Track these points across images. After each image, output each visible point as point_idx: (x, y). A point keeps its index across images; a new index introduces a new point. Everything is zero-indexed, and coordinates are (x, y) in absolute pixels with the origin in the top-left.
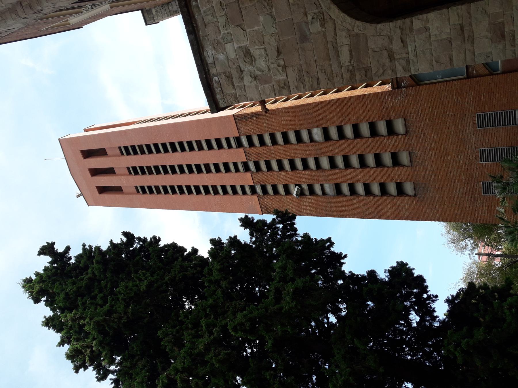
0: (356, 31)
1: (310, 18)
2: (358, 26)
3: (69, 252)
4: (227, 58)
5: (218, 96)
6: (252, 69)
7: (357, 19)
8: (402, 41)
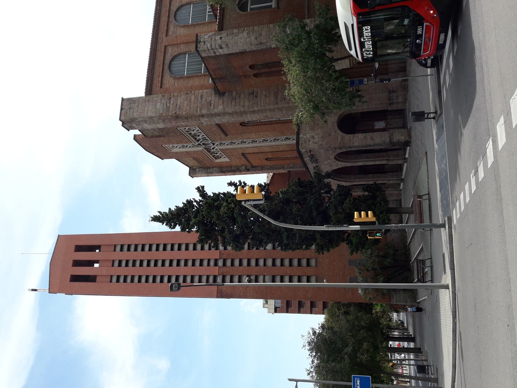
0: (343, 135)
1: (332, 131)
3: (175, 209)
5: (300, 146)
6: (313, 140)
7: (343, 133)
8: (353, 138)
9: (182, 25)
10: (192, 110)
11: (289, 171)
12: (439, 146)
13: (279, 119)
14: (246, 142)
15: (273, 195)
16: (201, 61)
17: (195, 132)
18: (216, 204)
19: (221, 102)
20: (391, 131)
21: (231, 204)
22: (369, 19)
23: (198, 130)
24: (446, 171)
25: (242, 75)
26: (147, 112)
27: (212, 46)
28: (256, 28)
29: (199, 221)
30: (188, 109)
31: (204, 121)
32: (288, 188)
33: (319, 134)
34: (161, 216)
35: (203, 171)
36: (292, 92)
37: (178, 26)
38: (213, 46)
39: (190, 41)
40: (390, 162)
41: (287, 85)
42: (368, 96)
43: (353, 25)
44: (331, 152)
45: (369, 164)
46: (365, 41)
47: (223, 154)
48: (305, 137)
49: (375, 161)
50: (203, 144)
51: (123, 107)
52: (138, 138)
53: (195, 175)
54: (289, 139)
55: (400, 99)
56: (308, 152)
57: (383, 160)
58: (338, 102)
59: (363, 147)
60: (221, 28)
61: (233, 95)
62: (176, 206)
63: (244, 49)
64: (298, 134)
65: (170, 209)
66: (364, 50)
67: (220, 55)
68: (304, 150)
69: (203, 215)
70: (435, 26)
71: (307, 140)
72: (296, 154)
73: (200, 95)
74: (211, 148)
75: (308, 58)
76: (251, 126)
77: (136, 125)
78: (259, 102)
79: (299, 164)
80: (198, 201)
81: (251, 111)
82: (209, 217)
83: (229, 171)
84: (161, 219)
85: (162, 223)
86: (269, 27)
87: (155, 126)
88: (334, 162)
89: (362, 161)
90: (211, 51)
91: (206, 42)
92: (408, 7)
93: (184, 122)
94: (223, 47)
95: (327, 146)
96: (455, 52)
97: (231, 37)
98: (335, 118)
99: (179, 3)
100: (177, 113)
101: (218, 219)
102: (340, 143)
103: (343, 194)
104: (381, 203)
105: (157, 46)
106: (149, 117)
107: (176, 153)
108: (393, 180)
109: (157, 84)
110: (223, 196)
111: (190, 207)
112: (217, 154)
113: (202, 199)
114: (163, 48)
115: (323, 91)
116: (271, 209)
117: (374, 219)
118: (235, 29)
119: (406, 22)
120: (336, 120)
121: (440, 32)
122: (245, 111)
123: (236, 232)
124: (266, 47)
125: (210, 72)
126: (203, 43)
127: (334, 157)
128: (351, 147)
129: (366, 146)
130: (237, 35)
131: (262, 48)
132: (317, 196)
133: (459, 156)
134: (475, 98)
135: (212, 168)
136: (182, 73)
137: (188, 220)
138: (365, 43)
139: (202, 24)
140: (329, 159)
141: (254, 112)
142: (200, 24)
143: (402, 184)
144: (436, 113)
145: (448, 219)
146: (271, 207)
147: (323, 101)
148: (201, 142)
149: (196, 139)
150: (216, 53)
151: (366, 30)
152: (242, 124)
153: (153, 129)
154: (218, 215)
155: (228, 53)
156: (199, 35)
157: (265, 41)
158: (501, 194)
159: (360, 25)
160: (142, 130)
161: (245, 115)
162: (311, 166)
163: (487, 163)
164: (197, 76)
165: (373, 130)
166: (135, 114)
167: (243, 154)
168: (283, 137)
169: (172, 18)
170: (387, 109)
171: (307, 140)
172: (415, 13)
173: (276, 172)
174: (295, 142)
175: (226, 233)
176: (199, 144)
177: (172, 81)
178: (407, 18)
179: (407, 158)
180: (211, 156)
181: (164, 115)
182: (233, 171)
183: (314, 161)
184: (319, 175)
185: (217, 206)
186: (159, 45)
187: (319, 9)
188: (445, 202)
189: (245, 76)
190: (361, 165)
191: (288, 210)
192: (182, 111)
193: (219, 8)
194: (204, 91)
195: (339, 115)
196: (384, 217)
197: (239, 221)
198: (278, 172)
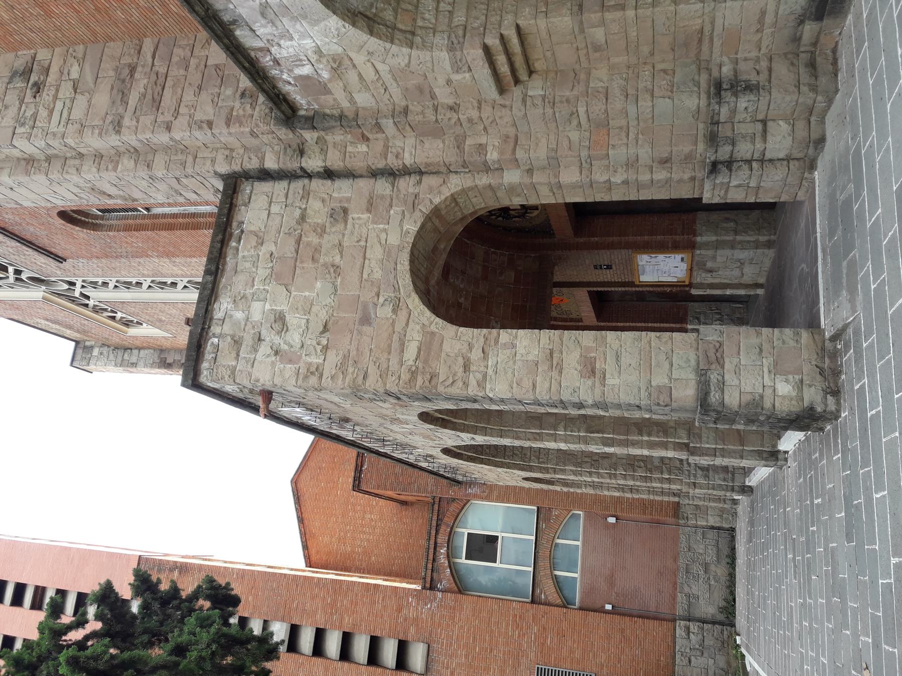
0: (433, 328)
2: (438, 324)
5: (205, 365)
6: (277, 340)
33: (314, 309)
35: (112, 357)
42: (582, 110)
71: (248, 340)
78: (43, 113)
95: (340, 382)
102: (413, 374)
120: (411, 239)
135: (136, 348)
170: (696, 196)
179: (786, 452)
195: (425, 208)
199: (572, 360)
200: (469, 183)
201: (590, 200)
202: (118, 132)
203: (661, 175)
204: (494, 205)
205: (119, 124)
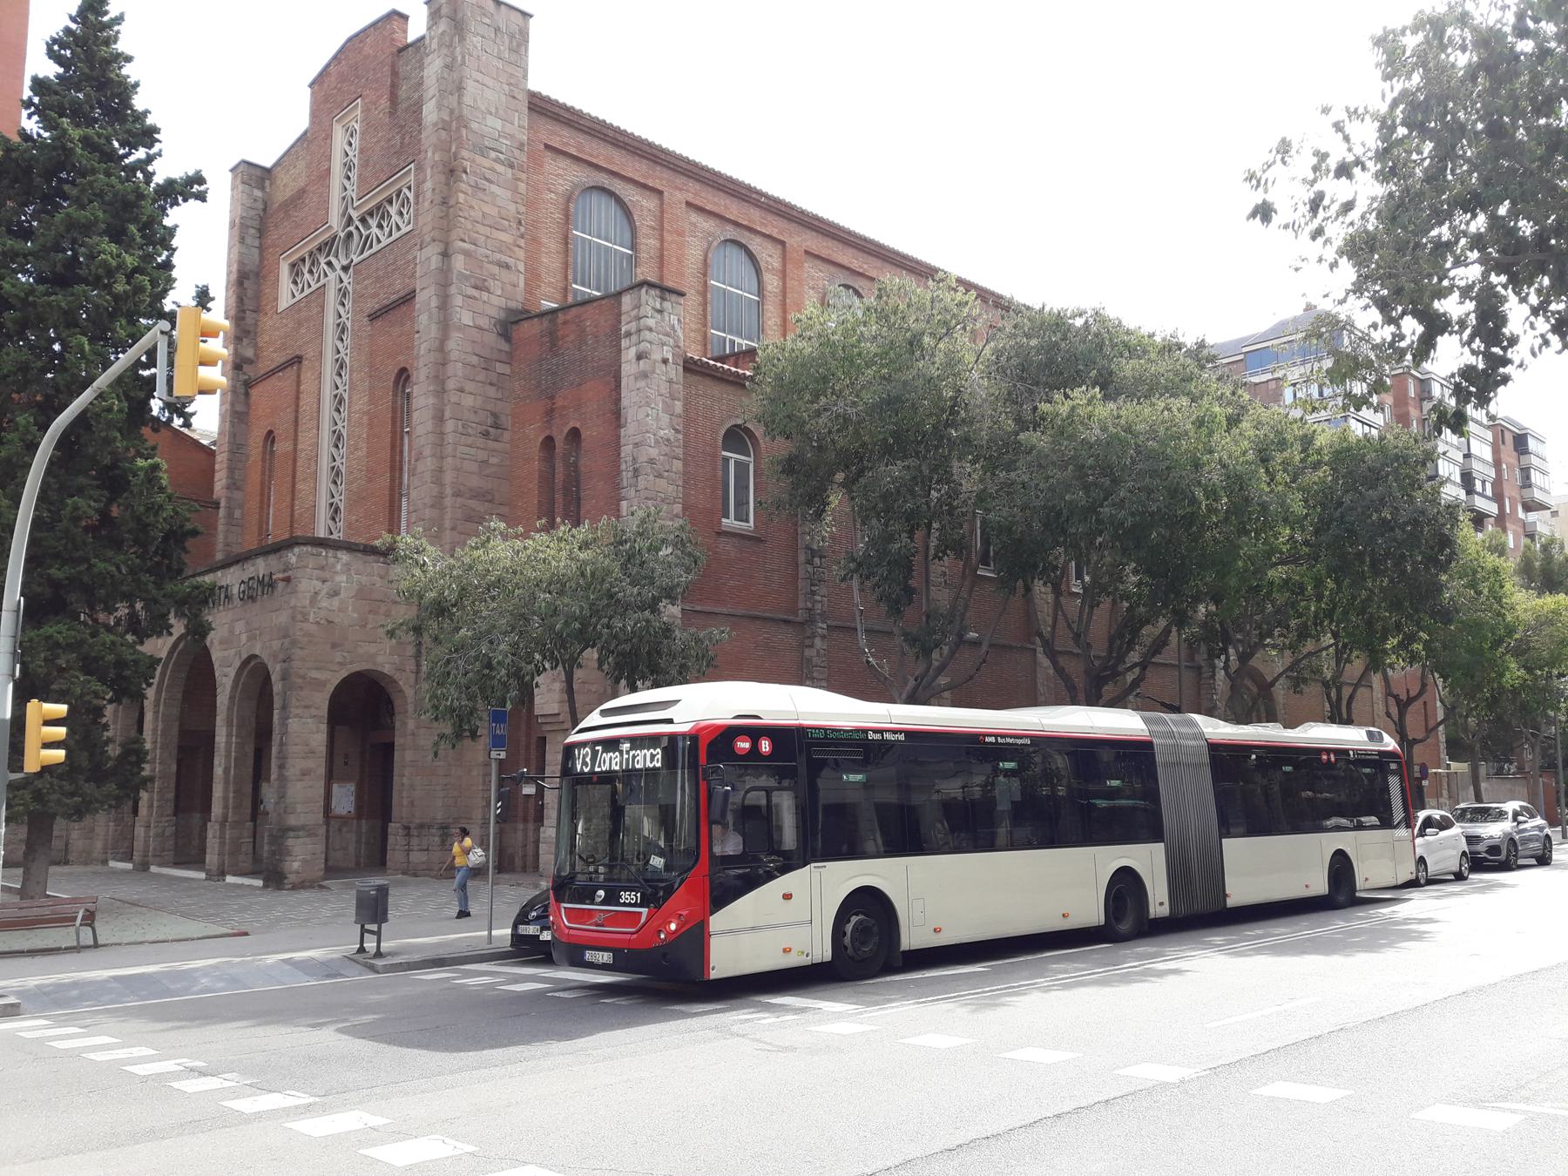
0: (328, 686)
1: (345, 654)
2: (331, 688)
4: (336, 573)
5: (309, 548)
6: (324, 592)
9: (710, 255)
10: (469, 226)
11: (217, 505)
12: (272, 966)
13: (408, 494)
14: (340, 375)
15: (145, 437)
16: (606, 287)
17: (395, 218)
18: (133, 228)
19: (484, 322)
20: (322, 831)
21: (128, 283)
22: (680, 765)
23: (399, 228)
24: (186, 991)
25: (554, 404)
26: (478, 81)
27: (647, 332)
28: (678, 465)
29: (69, 153)
30: (472, 213)
31: (429, 256)
32: (169, 491)
34: (106, 19)
35: (253, 213)
36: (497, 542)
37: (710, 244)
38: (647, 335)
39: (665, 271)
40: (217, 827)
41: (521, 529)
43: (670, 721)
44: (276, 645)
45: (216, 762)
46: (622, 755)
47: (307, 291)
48: (339, 567)
49: (226, 782)
50: (350, 235)
51: (503, 7)
52: (395, 24)
53: (239, 179)
54: (333, 519)
55: (417, 857)
56: (286, 574)
57: (224, 808)
58: (449, 674)
59: (281, 744)
60: (690, 367)
61: (498, 364)
62: (137, 85)
63: (629, 421)
64: (350, 547)
65: (129, 59)
66: (597, 748)
67: (620, 351)
68: (293, 560)
69: (93, 171)
70: (635, 936)
71: (326, 575)
72: (277, 533)
73: (511, 261)
74: (331, 258)
75: (588, 598)
76: (394, 402)
77: (442, 34)
78: (470, 440)
79: (240, 541)
80: (150, 169)
81: (442, 412)
82: (83, 191)
83: (240, 300)
84: (92, 17)
85: (74, 14)
86: (675, 503)
87: (431, 92)
88: (235, 655)
89: (228, 743)
90: (633, 326)
91: (659, 316)
92: (694, 866)
93: (433, 190)
94: (641, 362)
96: (556, 994)
97: (663, 391)
98: (387, 665)
99: (767, 262)
100: (464, 176)
101: (71, 224)
102: (303, 677)
103: (124, 674)
104: (73, 794)
105: (665, 169)
106: (461, 83)
107: (327, 135)
108: (147, 836)
109: (559, 136)
110: (159, 260)
111: (129, 132)
112: (311, 272)
113: (158, 185)
114: (658, 185)
115: (489, 632)
116: (93, 423)
117: (31, 765)
118: (685, 405)
119: (657, 862)
121: (616, 952)
122: (444, 391)
123: (8, 279)
124: (625, 485)
125: (574, 309)
126: (658, 306)
127: (257, 653)
128: (284, 707)
129: (283, 757)
130: (668, 409)
131: (624, 473)
132: (125, 588)
133: (244, 1023)
134: (433, 1050)
136: (580, 224)
137: (79, 115)
138: (617, 753)
139: (705, 316)
140: (252, 638)
141: (439, 418)
142: (705, 310)
143: (129, 866)
144: (379, 954)
145: (12, 1005)
146: (99, 423)
147: (458, 629)
148: (357, 228)
149: (371, 214)
150: (627, 340)
151: (653, 757)
152: (403, 376)
153: (420, 84)
154: (87, 228)
155: (623, 373)
156: (681, 300)
157: (641, 484)
158: (137, 1143)
159: (665, 742)
160: (419, 48)
161: (432, 388)
162: (232, 579)
163: (237, 1098)
164: (566, 265)
165: (330, 778)
166: (477, 40)
167: (298, 360)
168: (343, 497)
169: (731, 232)
171: (326, 575)
172: (676, 885)
173: (221, 461)
174: (321, 533)
175: (10, 242)
176: (350, 221)
177: (563, 186)
178: (666, 865)
179: (224, 880)
180: (304, 252)
181: (464, 131)
182: (241, 315)
183: (249, 588)
184: (207, 597)
185: (124, 231)
186: (666, 174)
187: (710, 639)
188: (75, 993)
189: (550, 413)
190: (217, 739)
191: (82, 480)
192: (470, 192)
193: (741, 371)
194: (522, 277)
195: (397, 676)
196: (23, 805)
197: (53, 298)
198: (217, 467)
199: (310, 764)
200: (409, 701)
201: (395, 765)
202: (453, 495)
203: (405, 802)
204: (397, 710)
205: (458, 495)
